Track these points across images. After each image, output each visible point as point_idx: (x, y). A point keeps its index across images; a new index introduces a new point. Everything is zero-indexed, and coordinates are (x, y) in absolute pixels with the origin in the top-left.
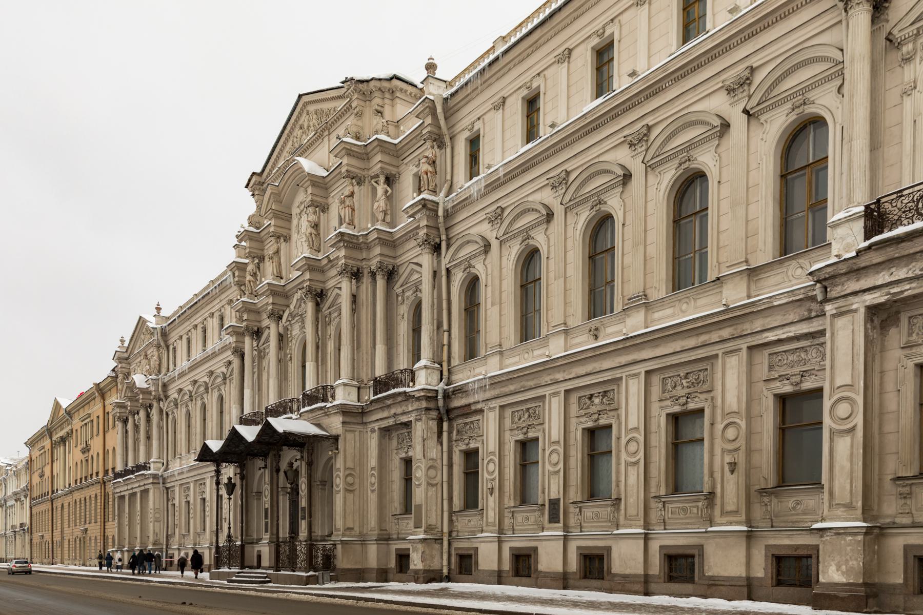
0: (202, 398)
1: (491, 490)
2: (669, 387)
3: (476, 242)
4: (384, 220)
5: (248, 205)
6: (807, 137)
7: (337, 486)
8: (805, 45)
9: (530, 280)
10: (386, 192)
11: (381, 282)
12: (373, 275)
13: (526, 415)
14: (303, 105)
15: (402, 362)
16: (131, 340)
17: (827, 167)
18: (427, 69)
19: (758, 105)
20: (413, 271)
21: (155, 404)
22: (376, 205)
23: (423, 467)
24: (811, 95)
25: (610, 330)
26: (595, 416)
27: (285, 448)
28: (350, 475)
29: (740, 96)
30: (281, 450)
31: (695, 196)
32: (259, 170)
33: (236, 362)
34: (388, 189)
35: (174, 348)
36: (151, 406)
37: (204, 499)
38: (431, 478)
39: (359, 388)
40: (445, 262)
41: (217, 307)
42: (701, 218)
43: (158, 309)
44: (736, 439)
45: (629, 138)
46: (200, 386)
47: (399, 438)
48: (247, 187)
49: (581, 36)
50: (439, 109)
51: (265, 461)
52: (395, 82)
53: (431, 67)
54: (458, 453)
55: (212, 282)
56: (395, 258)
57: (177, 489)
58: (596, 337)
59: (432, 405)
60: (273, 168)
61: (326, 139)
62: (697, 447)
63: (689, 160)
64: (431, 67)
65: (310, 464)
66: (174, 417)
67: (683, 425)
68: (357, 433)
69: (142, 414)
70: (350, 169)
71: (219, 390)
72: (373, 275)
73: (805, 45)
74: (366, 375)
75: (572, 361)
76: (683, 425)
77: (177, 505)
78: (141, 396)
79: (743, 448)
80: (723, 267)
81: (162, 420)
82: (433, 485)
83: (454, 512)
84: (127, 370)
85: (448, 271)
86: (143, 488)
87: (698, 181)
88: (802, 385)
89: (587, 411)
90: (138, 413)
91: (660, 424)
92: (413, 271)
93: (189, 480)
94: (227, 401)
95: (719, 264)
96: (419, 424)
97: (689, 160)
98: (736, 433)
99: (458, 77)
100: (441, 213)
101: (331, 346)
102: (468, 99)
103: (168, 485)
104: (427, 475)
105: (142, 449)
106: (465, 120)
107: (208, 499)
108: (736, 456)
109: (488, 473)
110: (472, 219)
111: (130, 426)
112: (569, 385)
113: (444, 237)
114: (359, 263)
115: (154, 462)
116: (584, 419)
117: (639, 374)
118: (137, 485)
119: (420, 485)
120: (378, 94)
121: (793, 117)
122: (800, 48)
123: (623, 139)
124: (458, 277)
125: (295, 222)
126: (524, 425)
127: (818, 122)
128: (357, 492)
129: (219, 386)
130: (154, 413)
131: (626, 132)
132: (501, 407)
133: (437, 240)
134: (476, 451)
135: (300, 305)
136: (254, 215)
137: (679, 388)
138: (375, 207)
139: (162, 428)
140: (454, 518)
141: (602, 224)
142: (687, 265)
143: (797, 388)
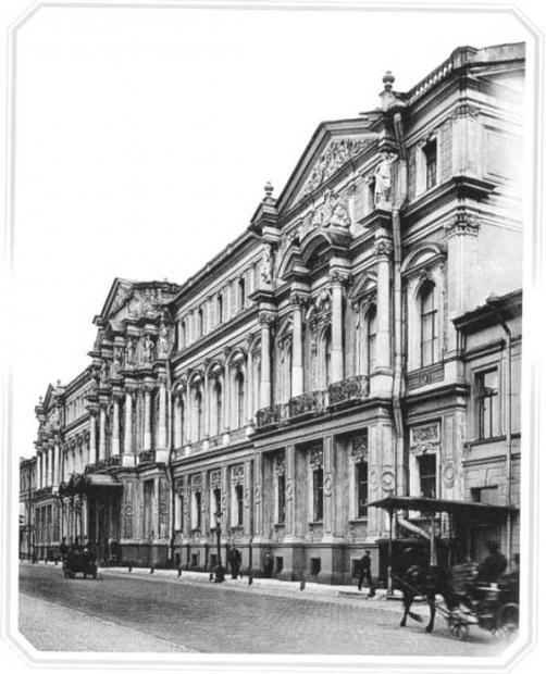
0: (181, 397)
3: (434, 251)
5: (95, 329)
12: (144, 393)
15: (50, 484)
18: (385, 81)
20: (369, 280)
41: (197, 304)
43: (389, 80)
53: (59, 382)
55: (191, 279)
56: (310, 292)
64: (59, 382)
92: (369, 280)
93: (222, 465)
99: (417, 88)
103: (176, 475)
106: (424, 126)
112: (231, 463)
134: (433, 457)
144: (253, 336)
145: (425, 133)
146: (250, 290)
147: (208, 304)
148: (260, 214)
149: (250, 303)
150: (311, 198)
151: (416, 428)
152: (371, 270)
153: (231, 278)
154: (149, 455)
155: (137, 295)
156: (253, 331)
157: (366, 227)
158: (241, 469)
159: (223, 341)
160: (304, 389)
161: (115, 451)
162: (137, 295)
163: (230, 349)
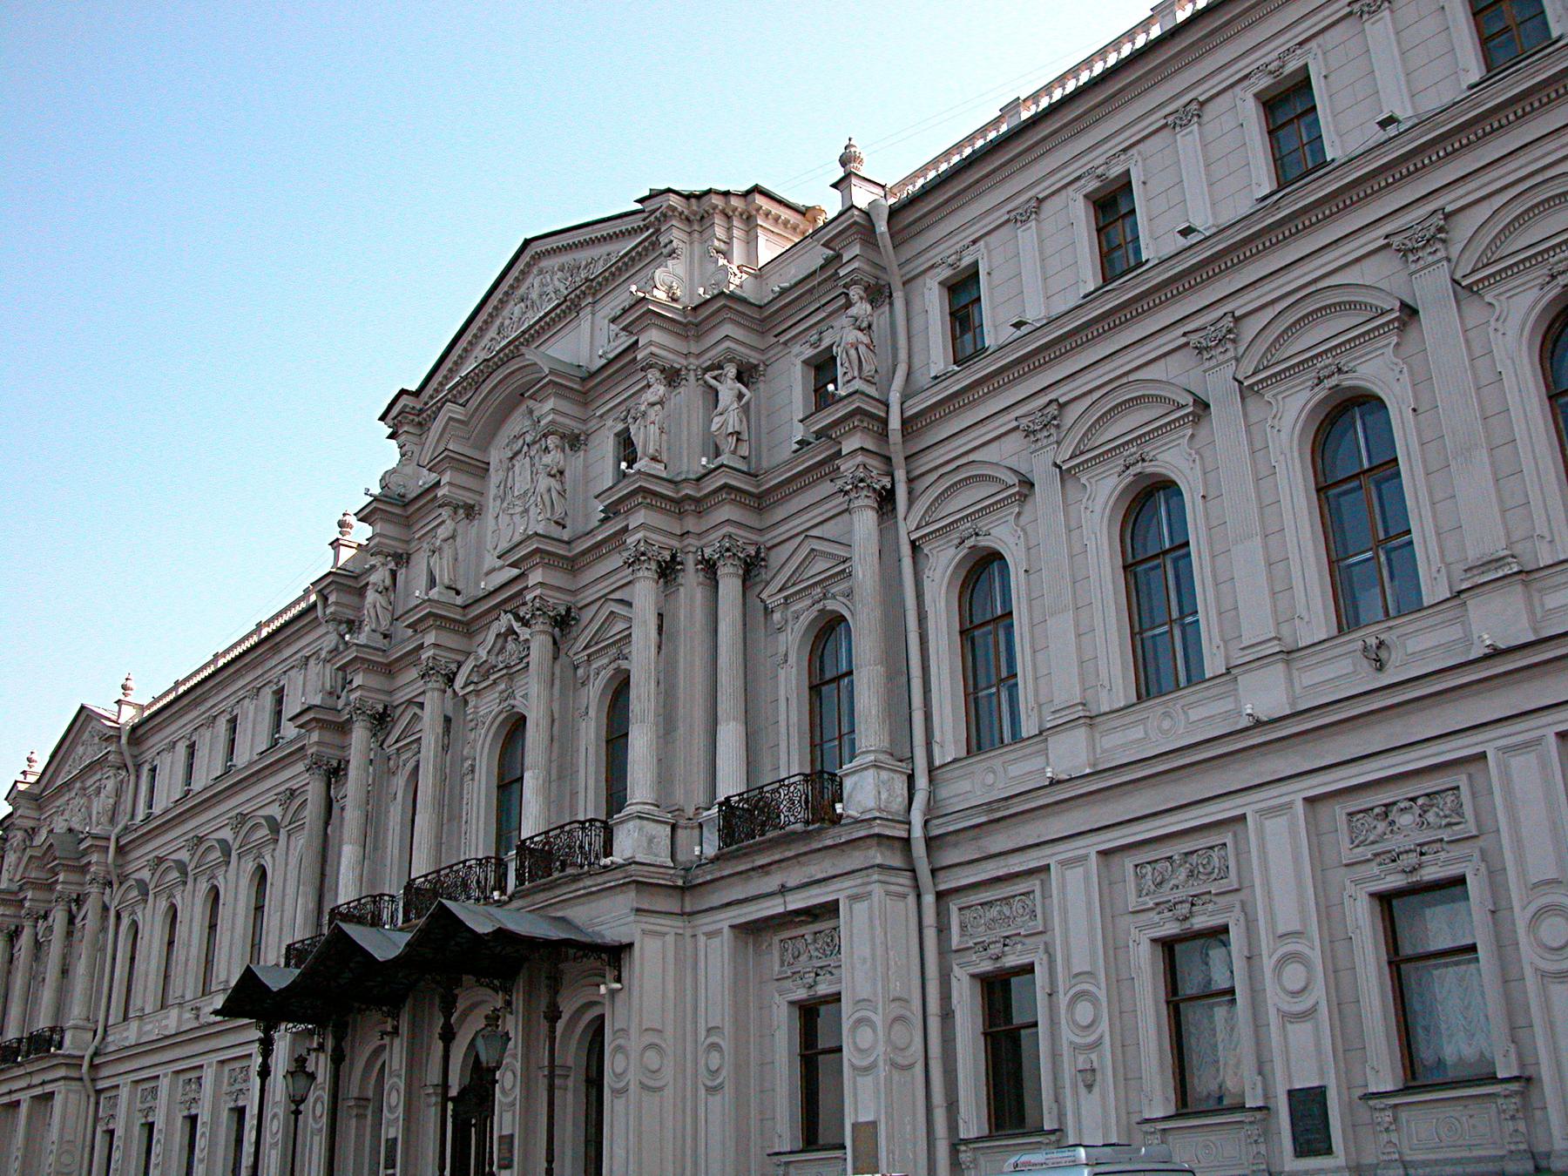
1: (1089, 1078)
2: (789, 957)
4: (734, 452)
6: (1157, 510)
7: (391, 1110)
8: (1320, 285)
9: (828, 676)
10: (740, 396)
11: (730, 585)
12: (710, 568)
13: (1182, 874)
14: (533, 257)
16: (53, 756)
17: (1398, 474)
19: (1473, 271)
21: (28, 924)
22: (717, 422)
23: (878, 1019)
24: (1149, 450)
25: (1413, 645)
26: (1184, 909)
27: (468, 979)
28: (651, 1046)
29: (1221, 358)
30: (459, 983)
31: (1159, 523)
32: (413, 387)
33: (314, 790)
34: (744, 389)
35: (154, 770)
36: (79, 901)
37: (151, 1126)
38: (897, 1049)
39: (674, 827)
40: (907, 524)
42: (1175, 561)
44: (1304, 989)
45: (1024, 421)
46: (257, 826)
47: (784, 950)
48: (382, 418)
49: (1259, 50)
50: (882, 227)
51: (396, 1017)
52: (760, 200)
54: (966, 980)
55: (1015, 105)
57: (124, 1093)
58: (1380, 665)
59: (74, 1073)
60: (447, 378)
61: (586, 314)
62: (1220, 1013)
63: (1143, 460)
65: (338, 1059)
66: (135, 924)
67: (1188, 970)
68: (670, 939)
69: (59, 917)
70: (560, 419)
71: (171, 896)
72: (710, 568)
73: (1320, 285)
74: (690, 794)
75: (1108, 782)
76: (1188, 970)
77: (119, 1133)
78: (61, 877)
79: (1323, 1008)
80: (1046, 710)
81: (104, 929)
82: (903, 1068)
83: (966, 1142)
84: (31, 824)
85: (915, 546)
86: (38, 1091)
87: (1161, 497)
88: (1004, 960)
89: (1378, 848)
90: (45, 917)
91: (1144, 963)
94: (146, 937)
95: (1040, 706)
96: (861, 908)
97: (1143, 460)
98: (1078, 1018)
100: (895, 423)
101: (395, 815)
102: (159, 728)
103: (101, 1085)
104: (889, 1041)
105: (47, 996)
107: (204, 1117)
108: (1094, 1056)
109: (1064, 1032)
110: (990, 425)
111: (25, 939)
112: (1317, 785)
113: (900, 475)
114: (675, 543)
115: (76, 1027)
116: (1374, 869)
117: (1085, 857)
118: (22, 1083)
119: (866, 1070)
120: (718, 220)
121: (1321, 393)
122: (1310, 290)
123: (1382, 242)
124: (944, 562)
125: (495, 477)
126: (1180, 894)
127: (994, 557)
128: (669, 1091)
129: (260, 846)
130: (91, 907)
131: (1389, 227)
132: (1104, 854)
133: (886, 481)
135: (503, 649)
136: (394, 471)
137: (804, 958)
138: (714, 427)
139: (103, 949)
140: (964, 1157)
141: (1149, 497)
142: (1162, 646)
143: (1187, 925)
144: (292, 793)
145: (945, 251)
146: (292, 707)
147: (208, 734)
148: (14, 793)
149: (289, 730)
150: (68, 785)
151: (964, 900)
152: (826, 530)
153: (214, 712)
154: (50, 1042)
155: (676, 235)
156: (294, 784)
157: (300, 727)
158: (155, 1089)
159: (150, 847)
160: (812, 762)
161: (589, 805)
162: (676, 235)
163: (201, 840)
